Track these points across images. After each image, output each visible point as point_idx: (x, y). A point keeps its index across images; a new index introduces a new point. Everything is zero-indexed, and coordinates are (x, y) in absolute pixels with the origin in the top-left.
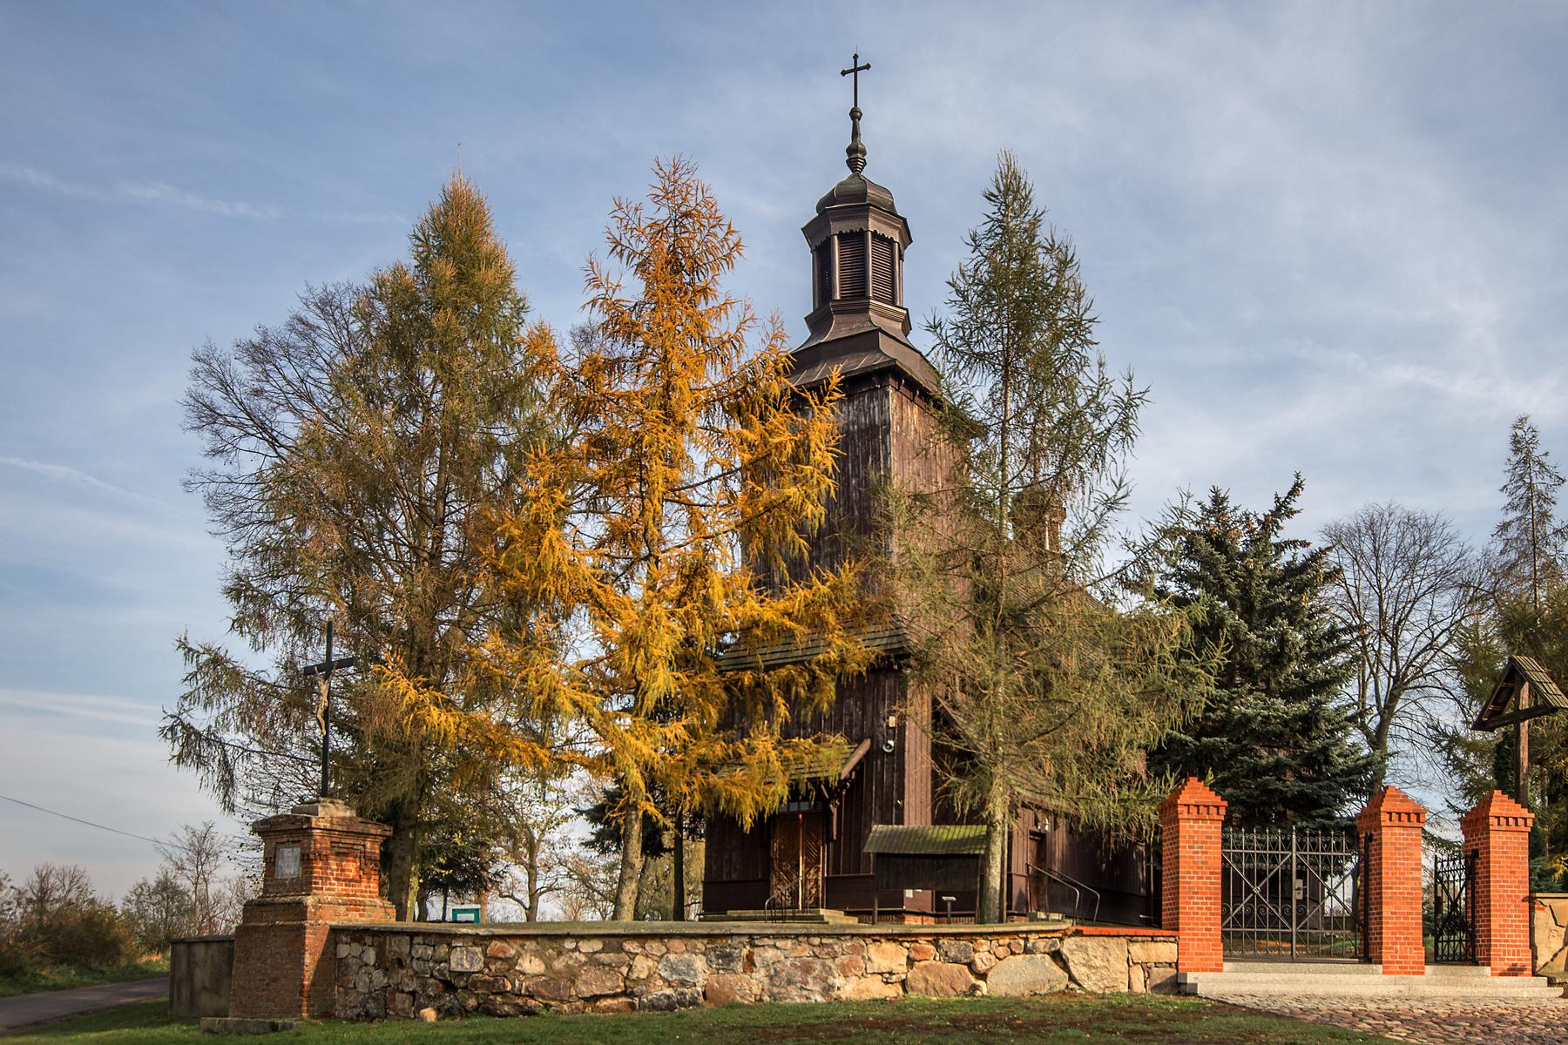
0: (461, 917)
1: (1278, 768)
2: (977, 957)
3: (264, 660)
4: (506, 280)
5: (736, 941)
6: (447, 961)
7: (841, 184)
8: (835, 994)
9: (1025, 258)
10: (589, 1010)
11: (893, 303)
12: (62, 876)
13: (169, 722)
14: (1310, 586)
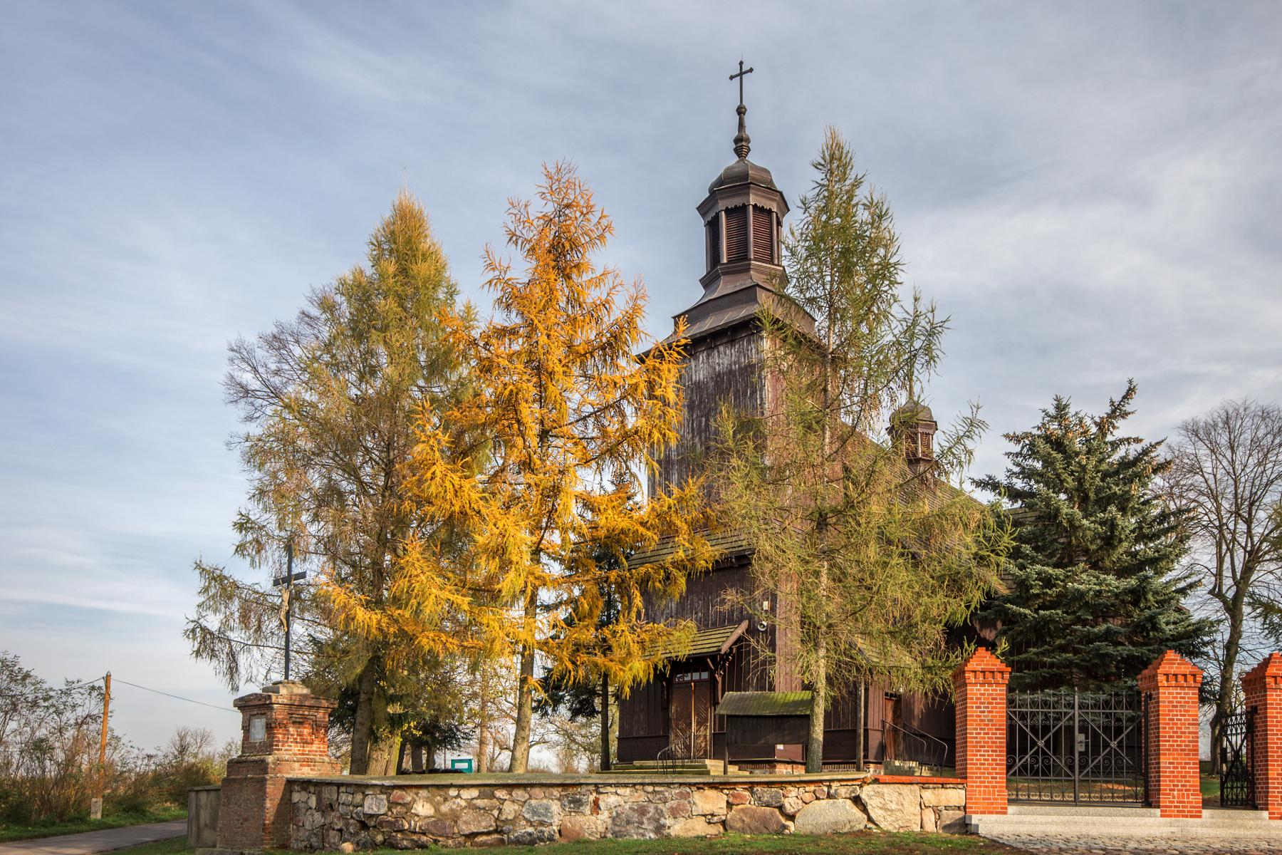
0: (458, 766)
1: (1108, 636)
2: (786, 802)
3: (258, 576)
4: (439, 271)
5: (584, 789)
6: (362, 806)
7: (728, 169)
8: (666, 832)
9: (847, 215)
10: (468, 844)
11: (772, 262)
12: (195, 736)
13: (191, 626)
14: (1141, 477)
